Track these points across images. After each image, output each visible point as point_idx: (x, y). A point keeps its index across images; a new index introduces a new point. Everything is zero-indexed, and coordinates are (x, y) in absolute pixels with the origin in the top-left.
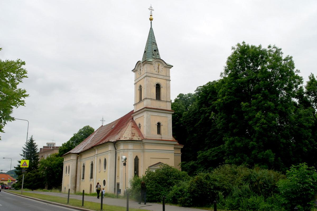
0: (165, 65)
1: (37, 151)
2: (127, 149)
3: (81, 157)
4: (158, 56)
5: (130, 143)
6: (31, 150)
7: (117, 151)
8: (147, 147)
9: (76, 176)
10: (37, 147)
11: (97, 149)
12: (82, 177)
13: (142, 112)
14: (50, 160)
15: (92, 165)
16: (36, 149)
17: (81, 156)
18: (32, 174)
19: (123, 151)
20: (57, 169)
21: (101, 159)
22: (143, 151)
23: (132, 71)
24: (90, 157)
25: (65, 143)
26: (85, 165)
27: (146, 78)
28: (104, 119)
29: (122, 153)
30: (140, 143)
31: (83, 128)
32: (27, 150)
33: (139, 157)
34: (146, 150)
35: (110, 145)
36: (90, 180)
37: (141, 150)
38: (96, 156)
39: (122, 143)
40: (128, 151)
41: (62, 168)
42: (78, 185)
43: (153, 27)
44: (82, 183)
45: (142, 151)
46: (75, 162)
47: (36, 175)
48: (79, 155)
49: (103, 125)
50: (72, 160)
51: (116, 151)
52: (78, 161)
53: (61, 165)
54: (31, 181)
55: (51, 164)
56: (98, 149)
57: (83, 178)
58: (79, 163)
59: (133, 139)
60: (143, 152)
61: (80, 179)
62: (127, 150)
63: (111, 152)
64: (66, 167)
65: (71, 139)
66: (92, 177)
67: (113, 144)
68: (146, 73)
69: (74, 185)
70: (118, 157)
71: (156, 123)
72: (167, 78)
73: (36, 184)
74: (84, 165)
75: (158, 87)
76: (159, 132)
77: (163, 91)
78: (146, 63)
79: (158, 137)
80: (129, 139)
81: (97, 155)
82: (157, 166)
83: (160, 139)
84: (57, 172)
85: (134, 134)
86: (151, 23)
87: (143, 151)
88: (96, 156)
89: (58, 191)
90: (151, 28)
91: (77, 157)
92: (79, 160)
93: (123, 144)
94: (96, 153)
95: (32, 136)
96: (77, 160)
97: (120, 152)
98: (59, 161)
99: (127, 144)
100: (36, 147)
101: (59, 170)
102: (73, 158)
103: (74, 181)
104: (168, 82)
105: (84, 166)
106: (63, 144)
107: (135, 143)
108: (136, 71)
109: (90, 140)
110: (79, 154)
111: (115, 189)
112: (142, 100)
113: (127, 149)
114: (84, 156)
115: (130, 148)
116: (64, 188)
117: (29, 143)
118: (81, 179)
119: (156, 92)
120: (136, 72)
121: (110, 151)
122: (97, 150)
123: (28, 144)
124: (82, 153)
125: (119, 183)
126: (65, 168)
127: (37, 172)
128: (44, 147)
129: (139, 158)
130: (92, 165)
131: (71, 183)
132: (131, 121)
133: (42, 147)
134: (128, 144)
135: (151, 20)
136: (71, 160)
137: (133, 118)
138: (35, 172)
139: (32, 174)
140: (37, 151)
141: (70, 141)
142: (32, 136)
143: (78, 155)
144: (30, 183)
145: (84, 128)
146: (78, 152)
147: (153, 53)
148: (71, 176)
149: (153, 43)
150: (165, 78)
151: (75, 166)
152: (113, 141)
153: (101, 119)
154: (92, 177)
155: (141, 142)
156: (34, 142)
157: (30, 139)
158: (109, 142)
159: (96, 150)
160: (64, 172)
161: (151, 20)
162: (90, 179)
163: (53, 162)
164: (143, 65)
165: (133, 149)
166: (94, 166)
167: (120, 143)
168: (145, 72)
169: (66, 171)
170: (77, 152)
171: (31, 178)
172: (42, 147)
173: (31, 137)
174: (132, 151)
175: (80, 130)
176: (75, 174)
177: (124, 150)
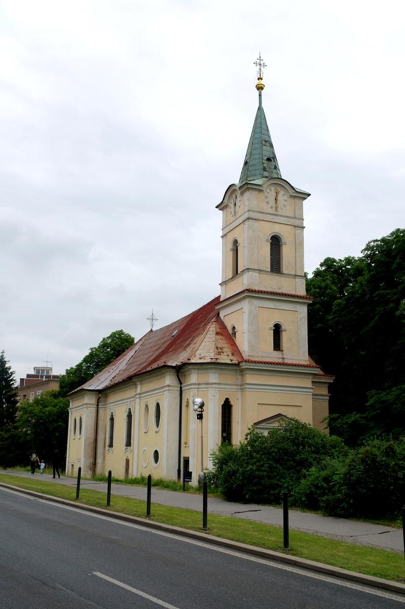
0: (291, 192)
2: (207, 384)
4: (275, 171)
7: (184, 386)
8: (250, 378)
10: (13, 376)
11: (141, 381)
12: (108, 443)
13: (239, 301)
15: (130, 416)
16: (12, 380)
17: (106, 396)
19: (197, 386)
22: (242, 387)
23: (216, 207)
24: (125, 399)
25: (72, 368)
26: (114, 417)
27: (247, 223)
31: (109, 335)
34: (247, 386)
38: (138, 396)
39: (194, 369)
40: (208, 388)
43: (263, 105)
44: (108, 456)
45: (239, 387)
46: (94, 410)
48: (102, 394)
50: (87, 404)
51: (181, 388)
52: (99, 406)
53: (64, 416)
55: (43, 413)
57: (111, 445)
59: (219, 361)
60: (241, 389)
61: (105, 447)
62: (207, 386)
63: (170, 388)
66: (129, 444)
67: (174, 370)
68: (249, 211)
69: (91, 460)
70: (186, 401)
71: (272, 324)
72: (297, 222)
74: (112, 416)
75: (276, 242)
76: (277, 346)
77: (286, 252)
78: (248, 189)
79: (275, 356)
80: (209, 361)
81: (140, 394)
83: (280, 361)
85: (220, 350)
86: (260, 95)
87: (242, 387)
90: (260, 109)
91: (98, 400)
92: (102, 406)
94: (139, 391)
95: (3, 352)
96: (98, 405)
97: (190, 389)
98: (60, 407)
99: (205, 371)
100: (11, 376)
101: (60, 426)
104: (298, 231)
105: (112, 419)
108: (227, 206)
110: (103, 393)
111: (179, 471)
112: (239, 272)
113: (207, 384)
114: (113, 398)
115: (213, 382)
119: (271, 255)
120: (225, 211)
121: (169, 386)
124: (108, 392)
126: (73, 421)
128: (28, 376)
129: (232, 403)
130: (130, 416)
131: (85, 456)
135: (260, 88)
136: (85, 406)
137: (219, 314)
141: (82, 363)
142: (3, 352)
143: (100, 395)
145: (113, 336)
146: (100, 388)
147: (265, 165)
148: (86, 441)
149: (263, 142)
150: (292, 222)
151: (94, 417)
152: (174, 365)
153: (149, 316)
154: (129, 444)
155: (238, 368)
158: (165, 367)
159: (137, 383)
161: (260, 88)
163: (47, 409)
164: (242, 194)
165: (220, 384)
167: (85, 394)
168: (246, 209)
169: (75, 428)
170: (97, 388)
172: (25, 377)
174: (215, 388)
175: (104, 339)
176: (92, 436)
177: (199, 384)
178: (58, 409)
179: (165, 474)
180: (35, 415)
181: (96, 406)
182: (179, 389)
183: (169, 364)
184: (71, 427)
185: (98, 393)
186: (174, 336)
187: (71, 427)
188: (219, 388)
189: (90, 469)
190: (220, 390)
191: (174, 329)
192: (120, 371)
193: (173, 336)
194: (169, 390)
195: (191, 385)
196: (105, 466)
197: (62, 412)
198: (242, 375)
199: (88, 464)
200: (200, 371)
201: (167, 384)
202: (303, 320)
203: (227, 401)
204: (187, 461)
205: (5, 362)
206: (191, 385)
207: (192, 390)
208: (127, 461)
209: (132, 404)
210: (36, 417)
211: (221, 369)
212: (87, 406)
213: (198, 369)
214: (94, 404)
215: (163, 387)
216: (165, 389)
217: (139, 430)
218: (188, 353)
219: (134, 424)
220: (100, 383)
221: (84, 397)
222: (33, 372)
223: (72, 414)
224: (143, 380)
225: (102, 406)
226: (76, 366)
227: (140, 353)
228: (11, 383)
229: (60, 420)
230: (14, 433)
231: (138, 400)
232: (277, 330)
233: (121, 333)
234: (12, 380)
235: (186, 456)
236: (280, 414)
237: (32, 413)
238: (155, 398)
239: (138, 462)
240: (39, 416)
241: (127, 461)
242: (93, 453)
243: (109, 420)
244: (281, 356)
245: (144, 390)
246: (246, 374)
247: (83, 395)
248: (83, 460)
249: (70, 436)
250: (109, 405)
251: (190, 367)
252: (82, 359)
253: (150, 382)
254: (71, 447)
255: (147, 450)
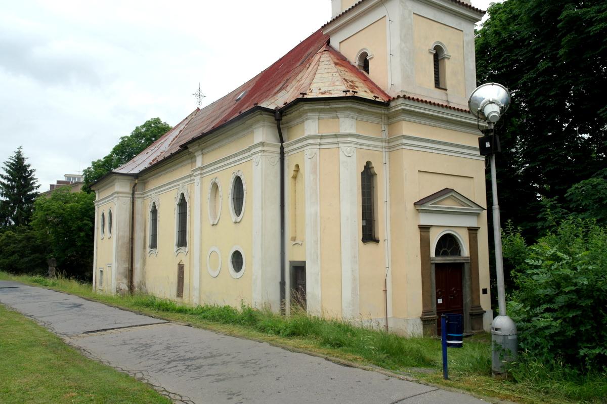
1: (34, 183)
2: (336, 136)
3: (144, 186)
5: (348, 113)
6: (20, 179)
7: (289, 145)
8: (407, 128)
9: (132, 239)
10: (32, 174)
11: (202, 150)
12: (149, 242)
14: (62, 200)
15: (183, 205)
16: (32, 179)
17: (145, 183)
18: (16, 235)
19: (318, 141)
20: (80, 223)
21: (217, 181)
22: (391, 144)
24: (173, 182)
25: (99, 161)
26: (157, 208)
28: (203, 92)
29: (315, 149)
30: (380, 116)
31: (143, 124)
32: (9, 180)
33: (377, 168)
34: (405, 141)
35: (261, 124)
36: (175, 250)
37: (382, 141)
38: (199, 172)
39: (313, 111)
40: (338, 143)
41: (92, 220)
42: (137, 265)
44: (150, 259)
45: (387, 145)
46: (127, 200)
47: (29, 239)
48: (140, 179)
49: (200, 109)
50: (118, 193)
51: (282, 148)
52: (136, 196)
53: (90, 213)
54: (14, 253)
55: (64, 210)
56: (204, 151)
57: (154, 245)
58: (138, 203)
60: (389, 148)
61: (144, 247)
62: (335, 140)
63: (265, 148)
64: (103, 213)
65: (114, 149)
66: (182, 241)
67: (271, 118)
69: (127, 265)
70: (293, 168)
73: (26, 259)
74: (154, 207)
76: (437, 84)
80: (343, 95)
81: (201, 169)
82: (441, 201)
83: (445, 104)
84: (80, 229)
87: (391, 144)
88: (199, 172)
89: (74, 284)
91: (134, 187)
92: (138, 196)
93: (316, 115)
94: (199, 164)
95: (20, 148)
96: (133, 194)
98: (85, 202)
99: (333, 115)
100: (30, 174)
101: (86, 225)
102: (121, 187)
103: (125, 254)
105: (154, 212)
106: (96, 163)
107: (362, 110)
109: (169, 142)
110: (140, 178)
111: (283, 284)
113: (336, 136)
114: (154, 183)
115: (348, 132)
116: (99, 274)
117: (12, 164)
118: (148, 249)
121: (263, 144)
122: (200, 152)
123: (10, 167)
124: (147, 176)
125: (305, 262)
126: (101, 217)
127: (29, 231)
128: (59, 182)
129: (376, 170)
130: (183, 205)
131: (117, 260)
132: (324, 48)
133: (55, 183)
134: (339, 114)
136: (115, 195)
137: (328, 42)
138: (25, 230)
139: (16, 235)
140: (34, 183)
141: (111, 156)
142: (20, 148)
143: (136, 181)
144: (12, 258)
145: (148, 125)
146: (136, 171)
148: (118, 240)
151: (128, 210)
152: (272, 107)
153: (195, 91)
154: (182, 241)
156: (26, 163)
157: (15, 154)
159: (196, 154)
160: (98, 228)
162: (176, 248)
163: (68, 205)
165: (358, 136)
166: (190, 207)
167: (306, 112)
169: (103, 225)
170: (132, 172)
171: (15, 244)
172: (55, 183)
173: (17, 150)
174: (350, 142)
175: (137, 128)
176: (127, 234)
177: (321, 137)
178: (82, 205)
179: (347, 294)
180: (53, 212)
181: (131, 196)
182: (279, 150)
183: (264, 105)
184: (98, 223)
185: (133, 178)
186: (240, 98)
187: (98, 223)
188: (358, 144)
189: (126, 277)
190: (358, 146)
191: (240, 93)
192: (162, 153)
193: (237, 100)
194: (263, 151)
195: (306, 139)
196: (145, 272)
197: (88, 208)
198: (389, 125)
199: (122, 270)
200: (323, 115)
201: (256, 142)
202: (470, 45)
203: (368, 163)
204: (299, 270)
205: (23, 158)
206: (306, 139)
207: (310, 147)
208: (181, 268)
209: (186, 187)
210: (54, 215)
211: (360, 112)
212: (119, 195)
213: (321, 111)
214: (128, 193)
215: (250, 149)
216: (253, 151)
217: (201, 222)
218: (290, 93)
219: (190, 215)
220: (135, 165)
221: (114, 185)
222: (64, 179)
223: (98, 208)
224: (207, 147)
225: (138, 196)
226: (104, 158)
227: (187, 132)
228: (31, 182)
229: (85, 218)
230: (29, 234)
231: (198, 179)
232: (438, 55)
233: (157, 121)
234: (32, 179)
235: (298, 258)
236: (447, 188)
237: (50, 210)
238: (235, 169)
239: (200, 269)
240: (58, 213)
241: (181, 268)
242: (129, 256)
243: (149, 212)
244: (445, 99)
245: (207, 163)
246: (402, 120)
247: (112, 181)
248: (114, 265)
249: (97, 237)
250: (149, 194)
251: (307, 107)
252: (112, 150)
253: (219, 147)
254: (99, 249)
255: (217, 250)
